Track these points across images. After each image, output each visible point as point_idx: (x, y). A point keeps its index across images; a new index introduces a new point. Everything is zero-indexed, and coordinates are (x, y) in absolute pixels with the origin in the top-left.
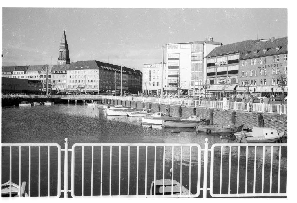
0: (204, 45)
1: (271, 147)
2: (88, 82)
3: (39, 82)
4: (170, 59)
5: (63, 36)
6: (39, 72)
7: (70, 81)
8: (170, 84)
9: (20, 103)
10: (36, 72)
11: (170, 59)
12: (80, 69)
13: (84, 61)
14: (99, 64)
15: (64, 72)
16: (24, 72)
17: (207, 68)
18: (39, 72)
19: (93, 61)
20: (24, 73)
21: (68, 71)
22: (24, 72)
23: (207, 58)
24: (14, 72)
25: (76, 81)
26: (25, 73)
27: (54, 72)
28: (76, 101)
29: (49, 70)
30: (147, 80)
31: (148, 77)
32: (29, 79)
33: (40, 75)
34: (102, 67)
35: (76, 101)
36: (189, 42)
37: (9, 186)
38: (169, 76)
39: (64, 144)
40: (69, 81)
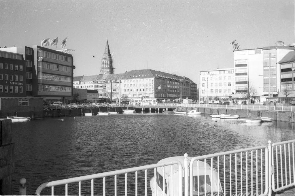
0: (277, 50)
1: (102, 178)
3: (96, 91)
4: (237, 66)
5: (106, 46)
6: (94, 82)
7: (125, 90)
8: (237, 91)
9: (86, 113)
10: (91, 82)
11: (237, 66)
12: (134, 78)
14: (152, 73)
15: (118, 81)
16: (78, 82)
17: (281, 74)
18: (93, 81)
20: (79, 83)
21: (123, 81)
22: (78, 82)
23: (280, 63)
25: (128, 90)
26: (80, 83)
27: (109, 82)
28: (150, 109)
29: (104, 80)
30: (205, 88)
31: (206, 85)
32: (89, 89)
33: (95, 84)
35: (150, 109)
36: (257, 48)
38: (237, 83)
39: (181, 154)
40: (124, 90)
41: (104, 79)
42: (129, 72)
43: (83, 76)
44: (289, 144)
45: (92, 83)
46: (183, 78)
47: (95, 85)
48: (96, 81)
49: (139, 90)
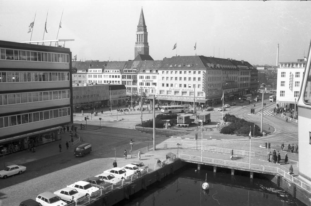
2: (171, 79)
6: (121, 72)
9: (272, 179)
13: (182, 57)
16: (101, 70)
18: (120, 70)
19: (196, 57)
20: (101, 71)
22: (101, 70)
24: (89, 70)
26: (103, 71)
34: (209, 65)
37: (3, 156)
41: (135, 67)
42: (169, 59)
43: (107, 61)
44: (141, 35)
45: (118, 72)
46: (242, 63)
47: (122, 75)
48: (124, 70)
49: (183, 86)
